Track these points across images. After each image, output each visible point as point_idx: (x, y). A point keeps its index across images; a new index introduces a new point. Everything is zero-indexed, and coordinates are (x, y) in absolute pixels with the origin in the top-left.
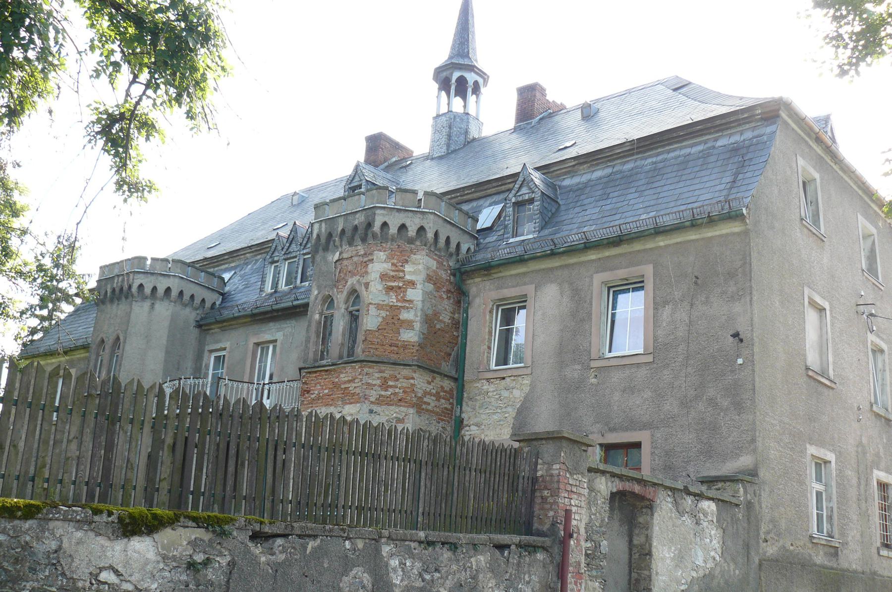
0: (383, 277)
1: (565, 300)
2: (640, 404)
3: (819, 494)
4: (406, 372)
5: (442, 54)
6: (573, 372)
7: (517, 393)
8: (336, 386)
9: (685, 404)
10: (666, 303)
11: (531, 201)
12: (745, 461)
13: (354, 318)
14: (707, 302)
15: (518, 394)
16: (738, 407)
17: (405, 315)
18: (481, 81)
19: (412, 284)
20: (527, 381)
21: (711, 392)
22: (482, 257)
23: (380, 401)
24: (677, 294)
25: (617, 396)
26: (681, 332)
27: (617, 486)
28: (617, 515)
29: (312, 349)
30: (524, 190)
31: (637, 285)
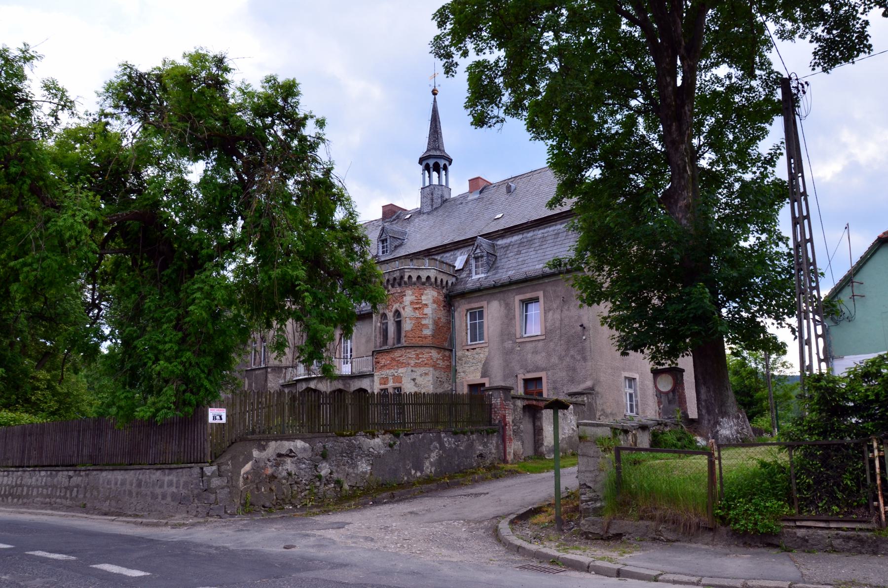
0: (412, 303)
1: (503, 309)
2: (540, 359)
3: (631, 395)
4: (427, 350)
5: (422, 147)
6: (508, 344)
7: (482, 355)
8: (393, 359)
9: (561, 358)
10: (550, 310)
11: (482, 257)
12: (589, 384)
13: (399, 324)
14: (568, 309)
15: (482, 356)
16: (585, 359)
17: (424, 322)
18: (447, 163)
19: (426, 305)
20: (487, 350)
21: (572, 353)
22: (460, 288)
23: (417, 365)
24: (555, 306)
25: (529, 356)
26: (558, 324)
27: (526, 403)
28: (527, 414)
29: (378, 341)
30: (478, 251)
31: (536, 300)
